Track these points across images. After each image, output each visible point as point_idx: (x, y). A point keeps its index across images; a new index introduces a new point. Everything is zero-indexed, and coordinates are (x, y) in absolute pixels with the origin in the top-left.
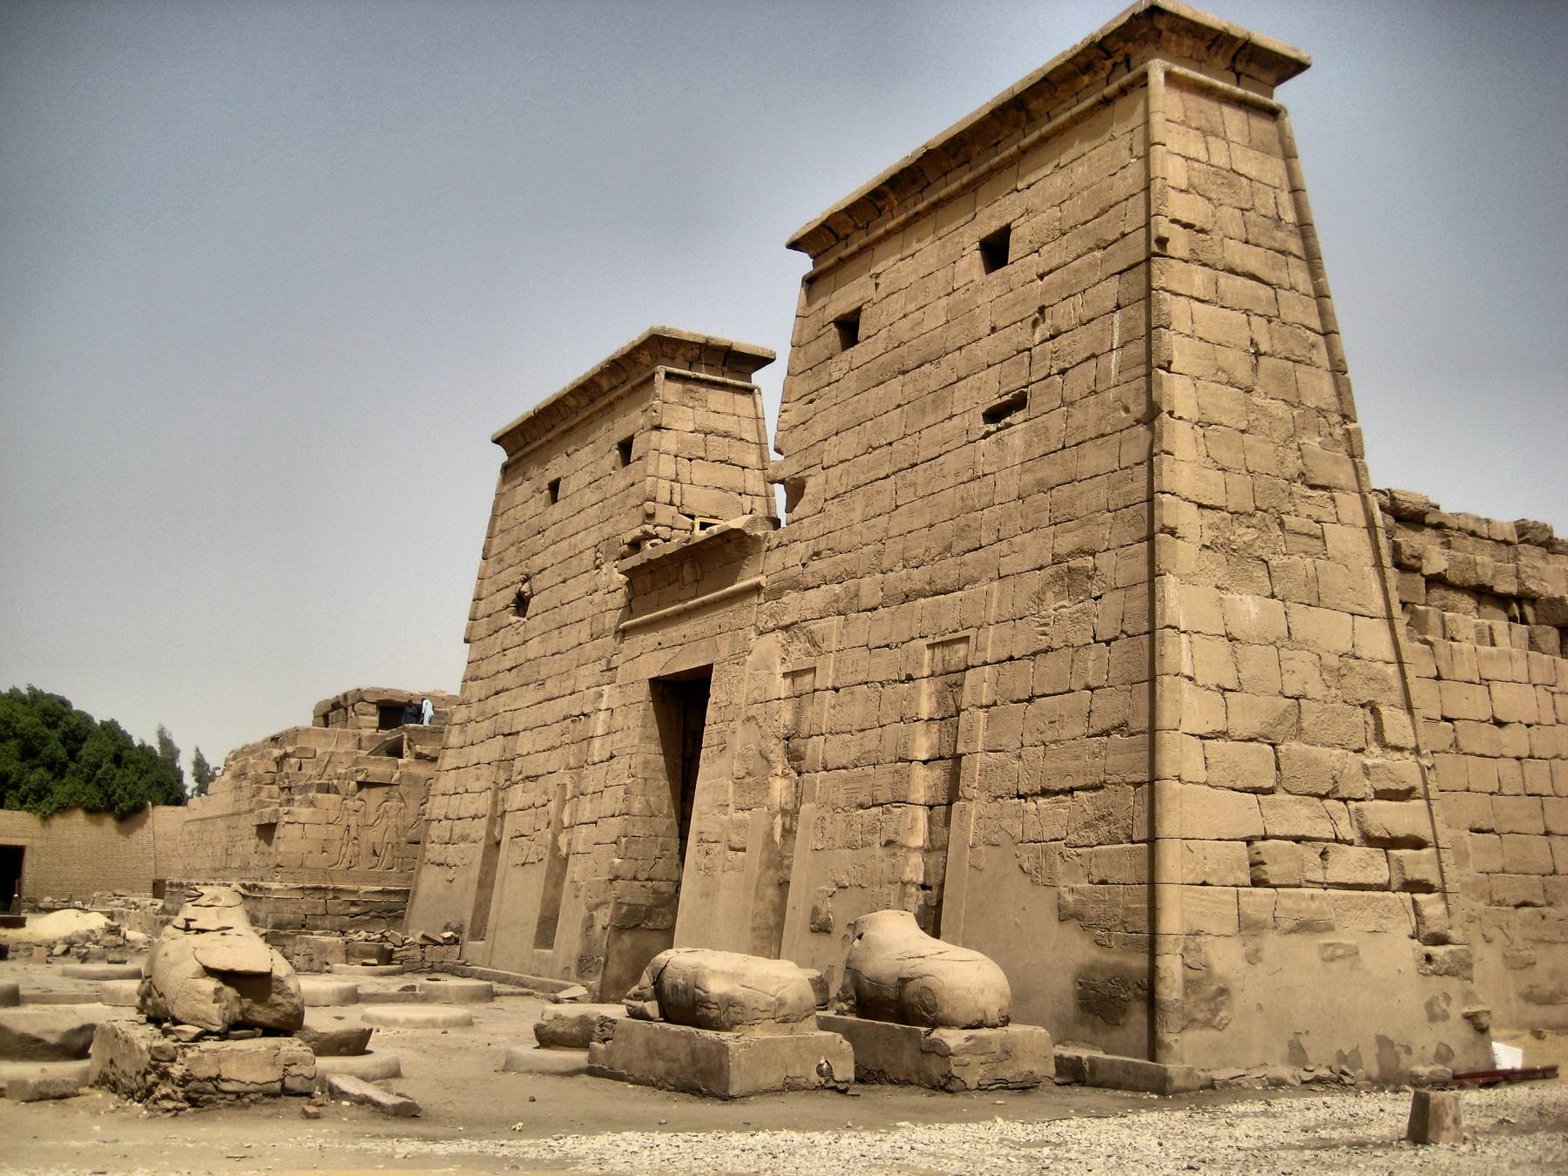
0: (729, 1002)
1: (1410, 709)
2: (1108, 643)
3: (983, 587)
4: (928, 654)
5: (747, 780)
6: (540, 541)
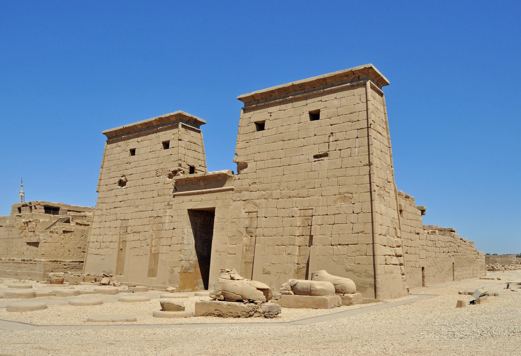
0: (320, 290)
1: (400, 229)
3: (316, 197)
5: (233, 237)
6: (128, 166)
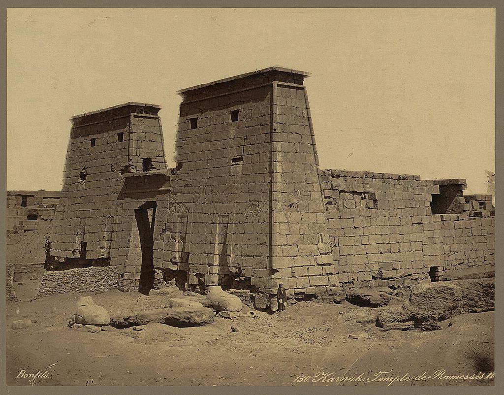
2: (261, 223)
4: (218, 218)
